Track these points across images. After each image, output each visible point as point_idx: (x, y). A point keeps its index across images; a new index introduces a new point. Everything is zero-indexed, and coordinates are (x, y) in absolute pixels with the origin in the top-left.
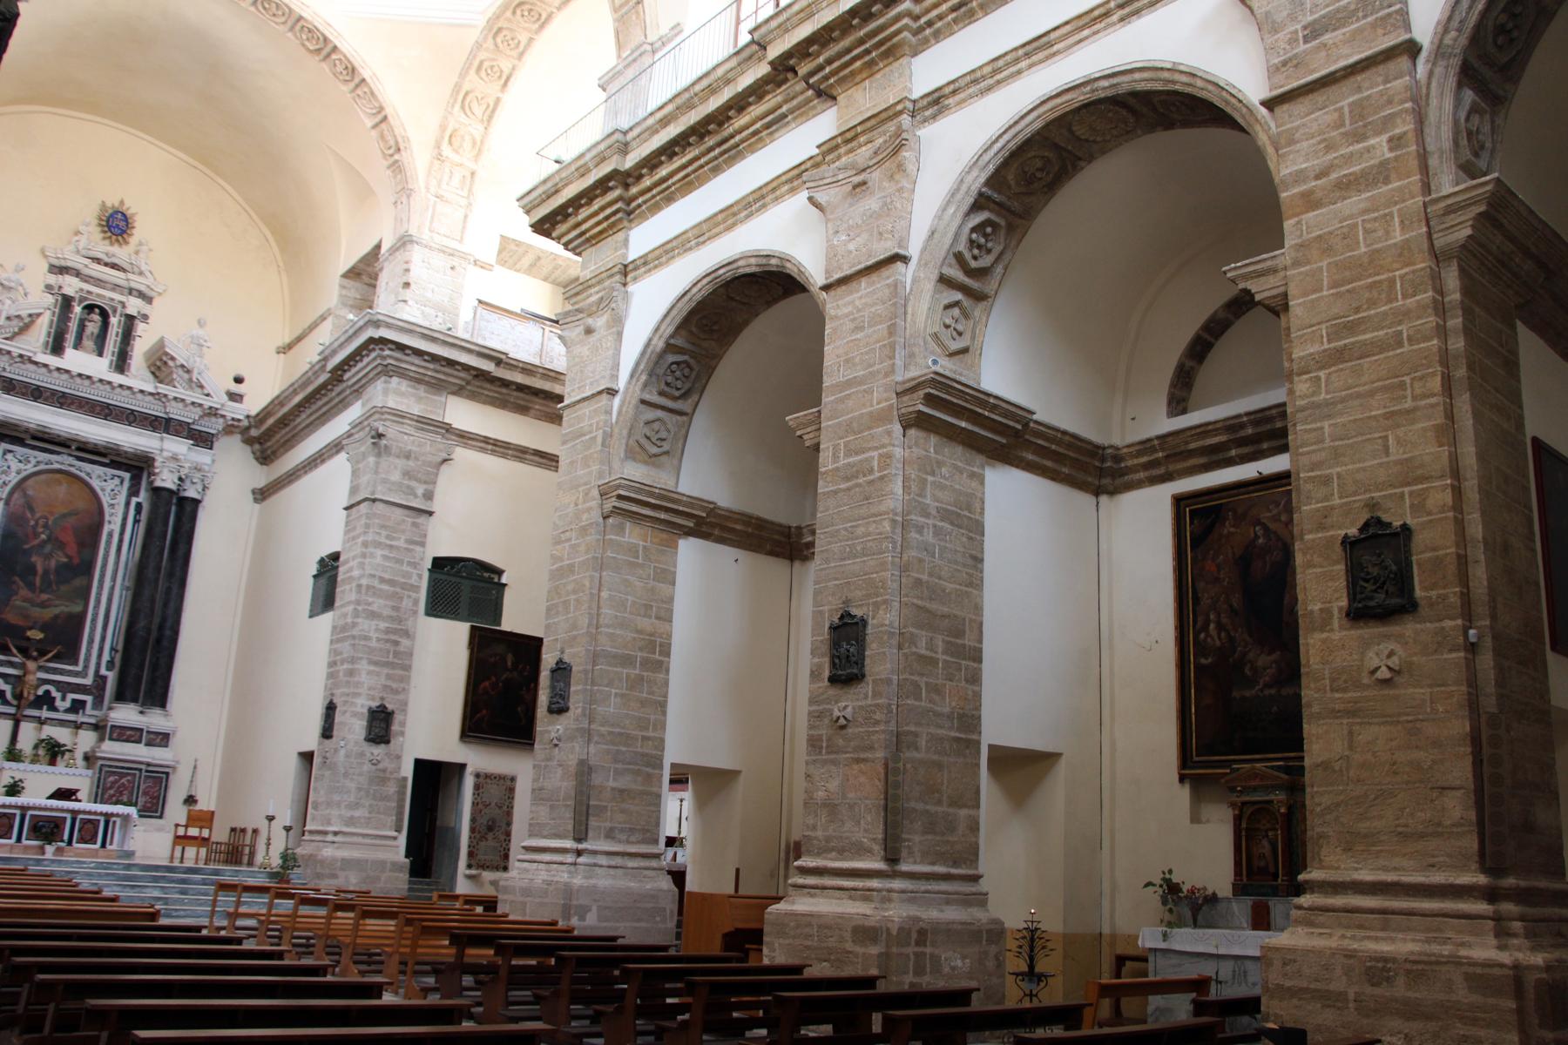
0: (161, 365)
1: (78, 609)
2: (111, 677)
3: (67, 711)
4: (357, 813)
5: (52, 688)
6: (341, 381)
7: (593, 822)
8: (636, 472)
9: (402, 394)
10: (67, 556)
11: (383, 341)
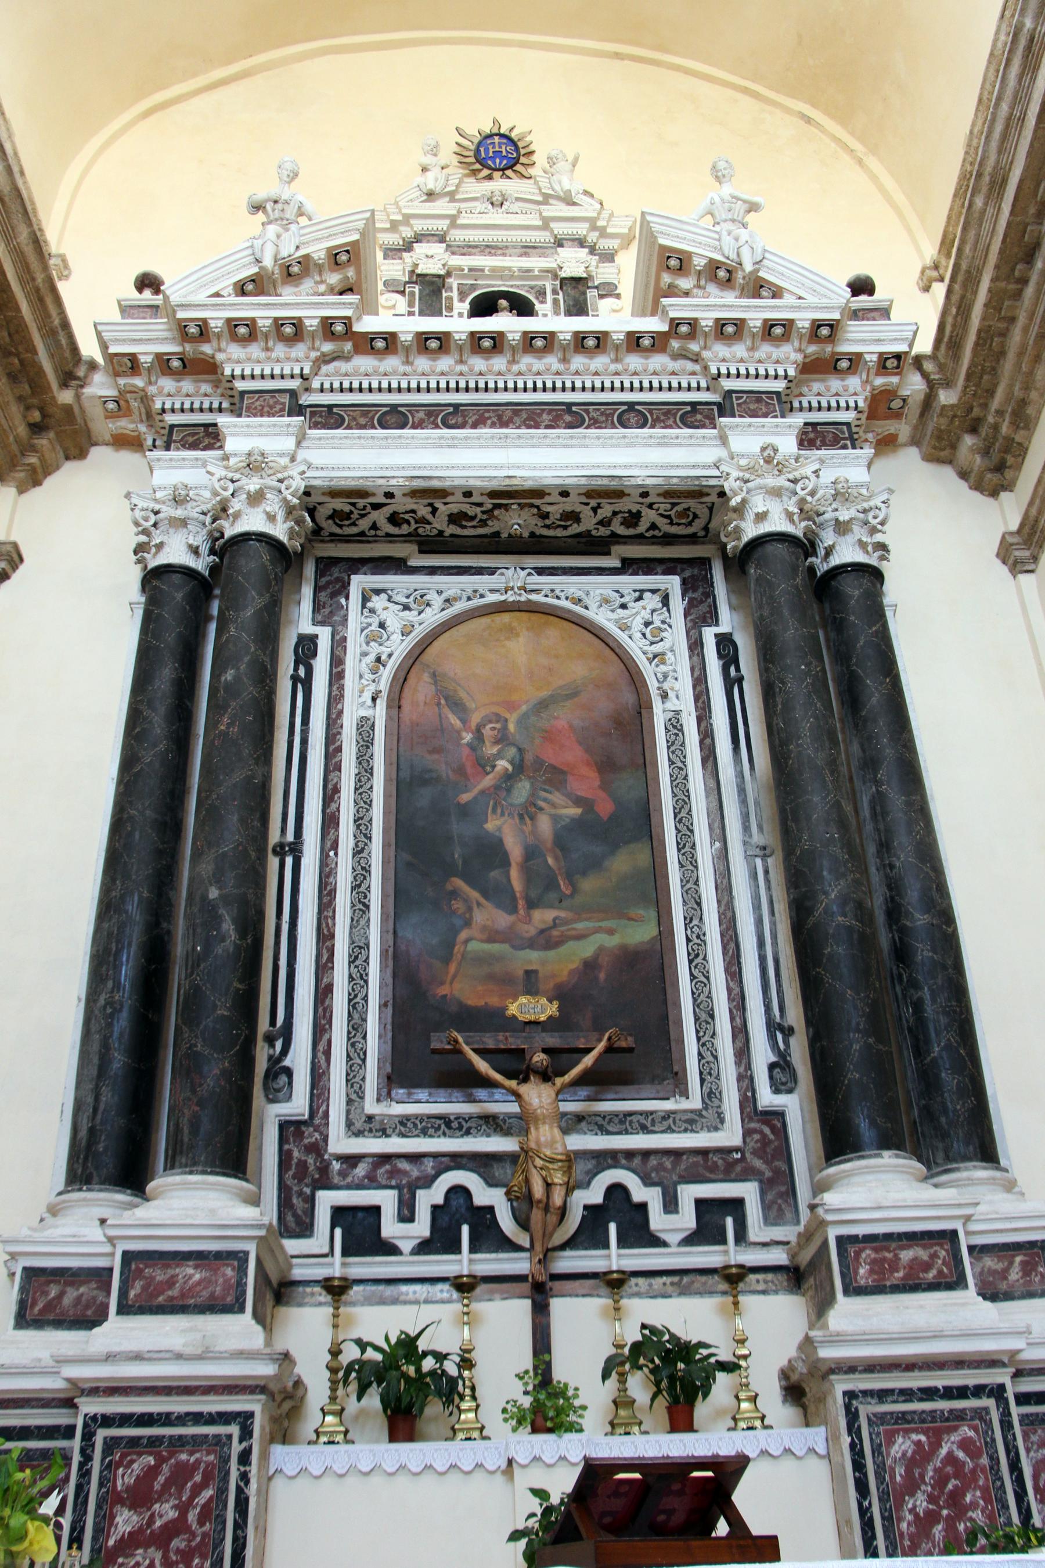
1: (640, 933)
2: (796, 1108)
3: (424, 1247)
10: (578, 801)
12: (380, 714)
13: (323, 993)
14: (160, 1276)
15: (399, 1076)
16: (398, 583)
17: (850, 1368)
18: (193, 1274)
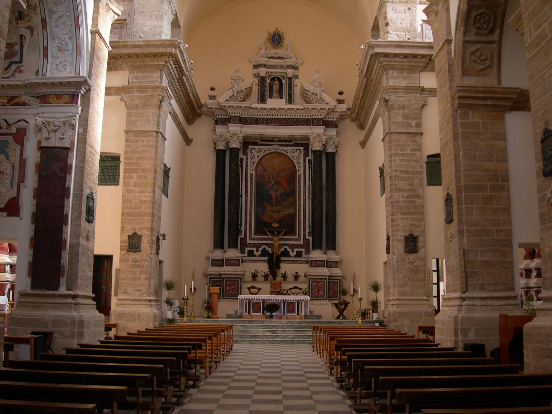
0: (306, 97)
1: (291, 211)
3: (295, 256)
4: (405, 289)
5: (287, 248)
6: (372, 80)
7: (470, 281)
8: (471, 81)
9: (395, 78)
10: (284, 189)
11: (377, 55)
12: (254, 173)
13: (246, 219)
14: (229, 262)
15: (257, 232)
16: (257, 147)
17: (310, 276)
18: (233, 261)
